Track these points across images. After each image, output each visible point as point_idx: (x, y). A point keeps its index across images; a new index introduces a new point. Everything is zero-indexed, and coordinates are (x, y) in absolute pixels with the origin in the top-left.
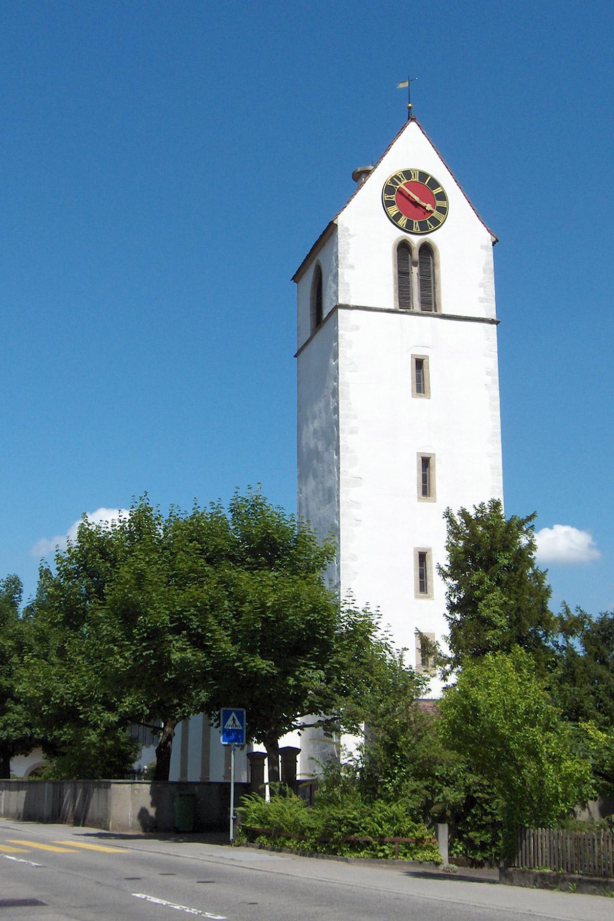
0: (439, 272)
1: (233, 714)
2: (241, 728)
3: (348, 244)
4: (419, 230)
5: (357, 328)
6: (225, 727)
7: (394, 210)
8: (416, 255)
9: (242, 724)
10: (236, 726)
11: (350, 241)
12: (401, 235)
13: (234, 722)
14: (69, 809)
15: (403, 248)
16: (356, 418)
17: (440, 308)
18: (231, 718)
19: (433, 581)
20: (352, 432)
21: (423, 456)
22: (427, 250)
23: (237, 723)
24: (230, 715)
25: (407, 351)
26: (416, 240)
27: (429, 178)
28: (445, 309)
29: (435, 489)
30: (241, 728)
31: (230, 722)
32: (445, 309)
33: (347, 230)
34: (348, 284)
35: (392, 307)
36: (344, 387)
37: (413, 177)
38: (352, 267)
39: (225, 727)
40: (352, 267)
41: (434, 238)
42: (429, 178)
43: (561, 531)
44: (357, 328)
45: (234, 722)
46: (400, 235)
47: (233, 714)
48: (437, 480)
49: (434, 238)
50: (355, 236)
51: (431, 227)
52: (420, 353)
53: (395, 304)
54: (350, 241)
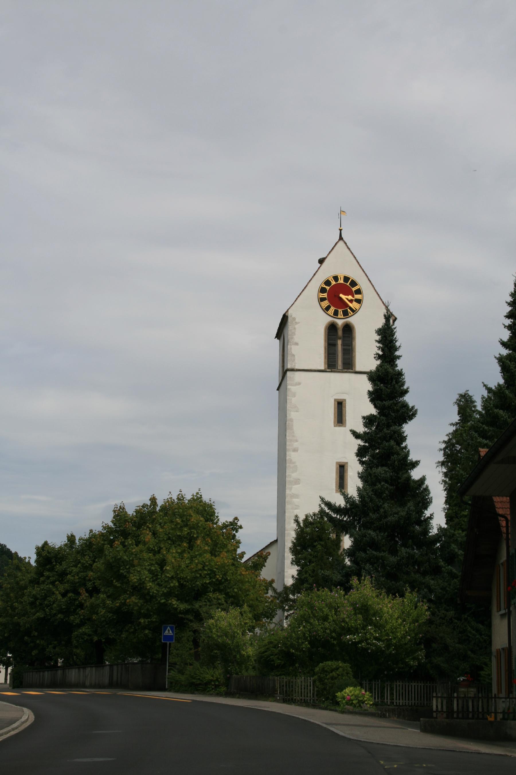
0: (355, 343)
1: (169, 628)
2: (172, 634)
3: (295, 329)
4: (342, 316)
5: (299, 384)
6: (164, 634)
7: (326, 303)
8: (340, 333)
9: (173, 632)
10: (170, 633)
11: (296, 326)
12: (331, 319)
13: (169, 632)
14: (200, 687)
15: (332, 328)
16: (297, 441)
17: (355, 367)
18: (167, 630)
19: (344, 543)
20: (295, 450)
21: (341, 464)
22: (348, 329)
23: (171, 632)
24: (167, 628)
25: (332, 397)
26: (340, 323)
27: (351, 280)
28: (358, 368)
29: (347, 485)
30: (172, 634)
31: (167, 632)
32: (358, 368)
33: (294, 319)
34: (294, 355)
35: (322, 368)
36: (290, 422)
37: (339, 280)
38: (297, 344)
39: (164, 634)
40: (297, 344)
41: (353, 320)
42: (351, 280)
43: (34, 651)
44: (299, 384)
45: (169, 632)
46: (330, 319)
47: (169, 628)
48: (348, 480)
49: (353, 320)
50: (299, 323)
51: (350, 313)
52: (340, 397)
53: (325, 366)
54: (296, 326)
